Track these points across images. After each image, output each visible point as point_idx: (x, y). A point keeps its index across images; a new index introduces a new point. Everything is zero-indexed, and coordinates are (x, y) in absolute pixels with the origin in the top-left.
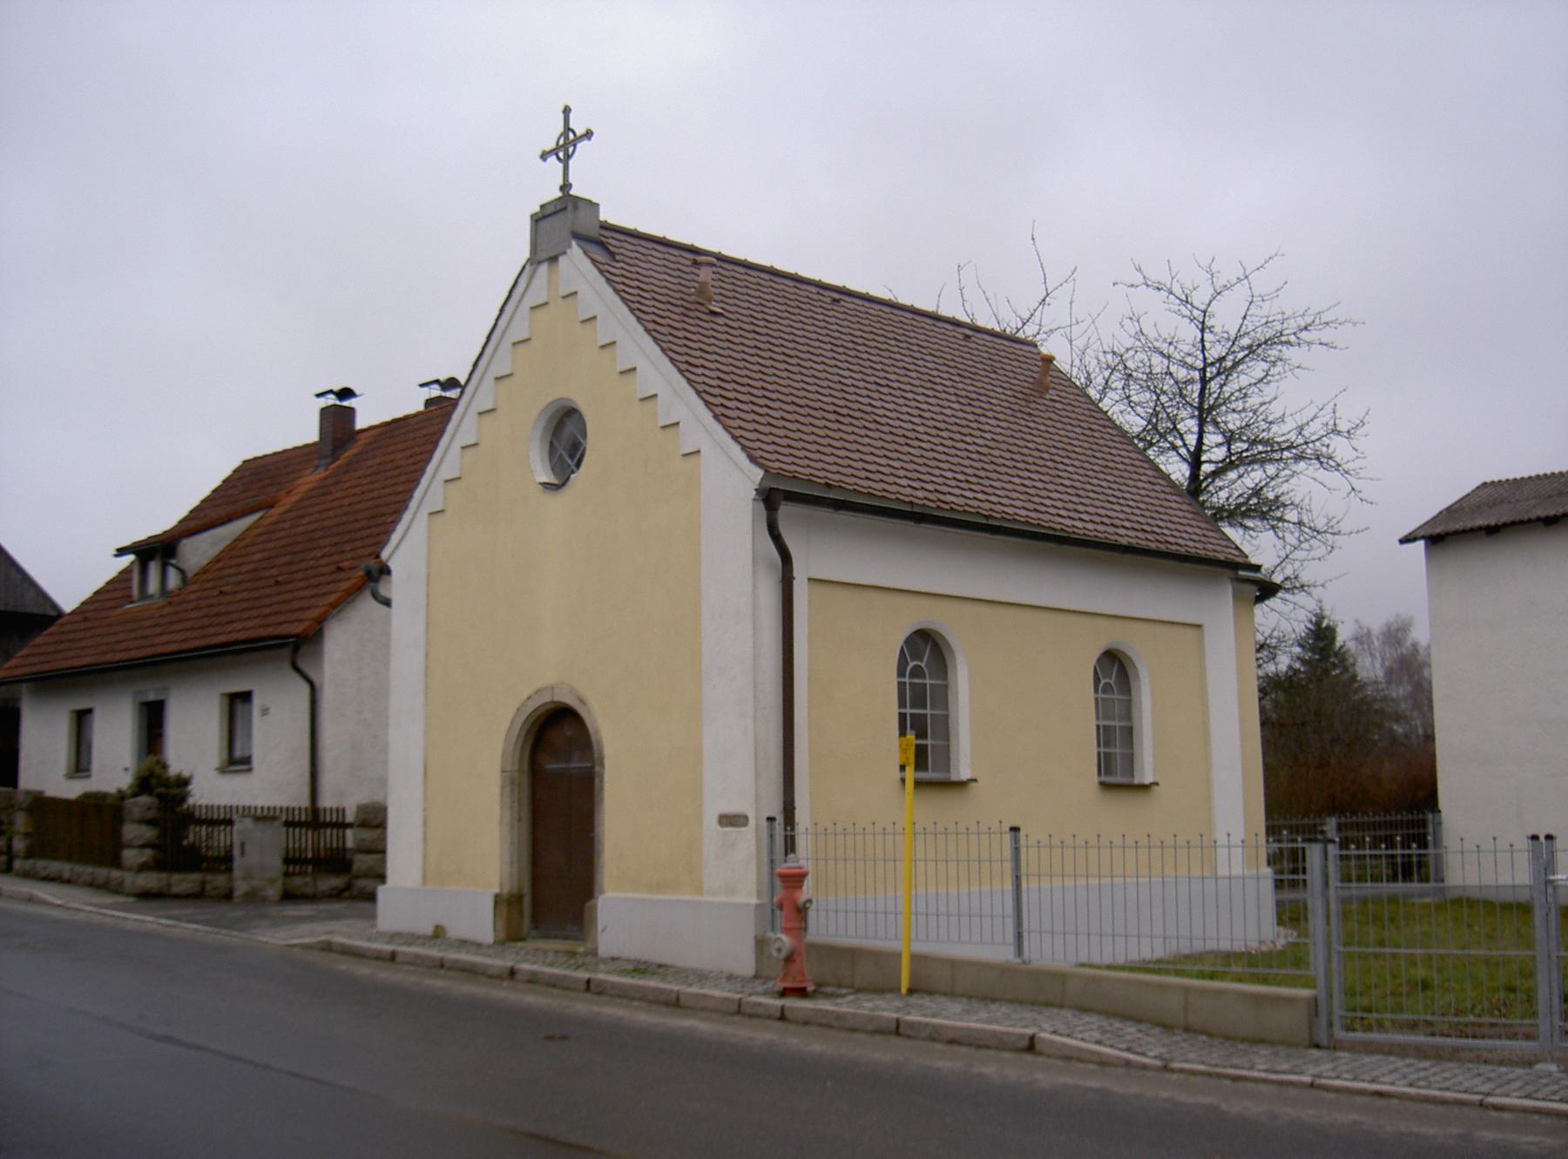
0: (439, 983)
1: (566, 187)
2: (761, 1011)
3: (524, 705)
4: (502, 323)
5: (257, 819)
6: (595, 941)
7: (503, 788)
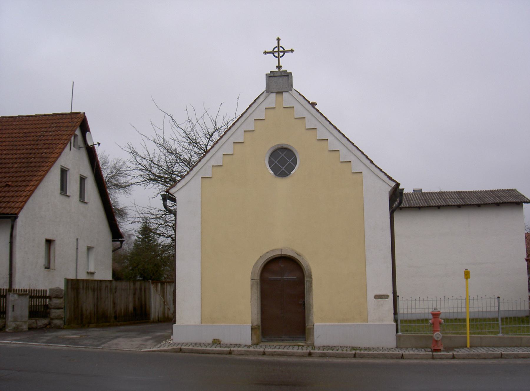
0: (277, 359)
1: (279, 67)
2: (443, 357)
3: (265, 255)
4: (250, 111)
5: (19, 295)
6: (313, 341)
7: (252, 286)
